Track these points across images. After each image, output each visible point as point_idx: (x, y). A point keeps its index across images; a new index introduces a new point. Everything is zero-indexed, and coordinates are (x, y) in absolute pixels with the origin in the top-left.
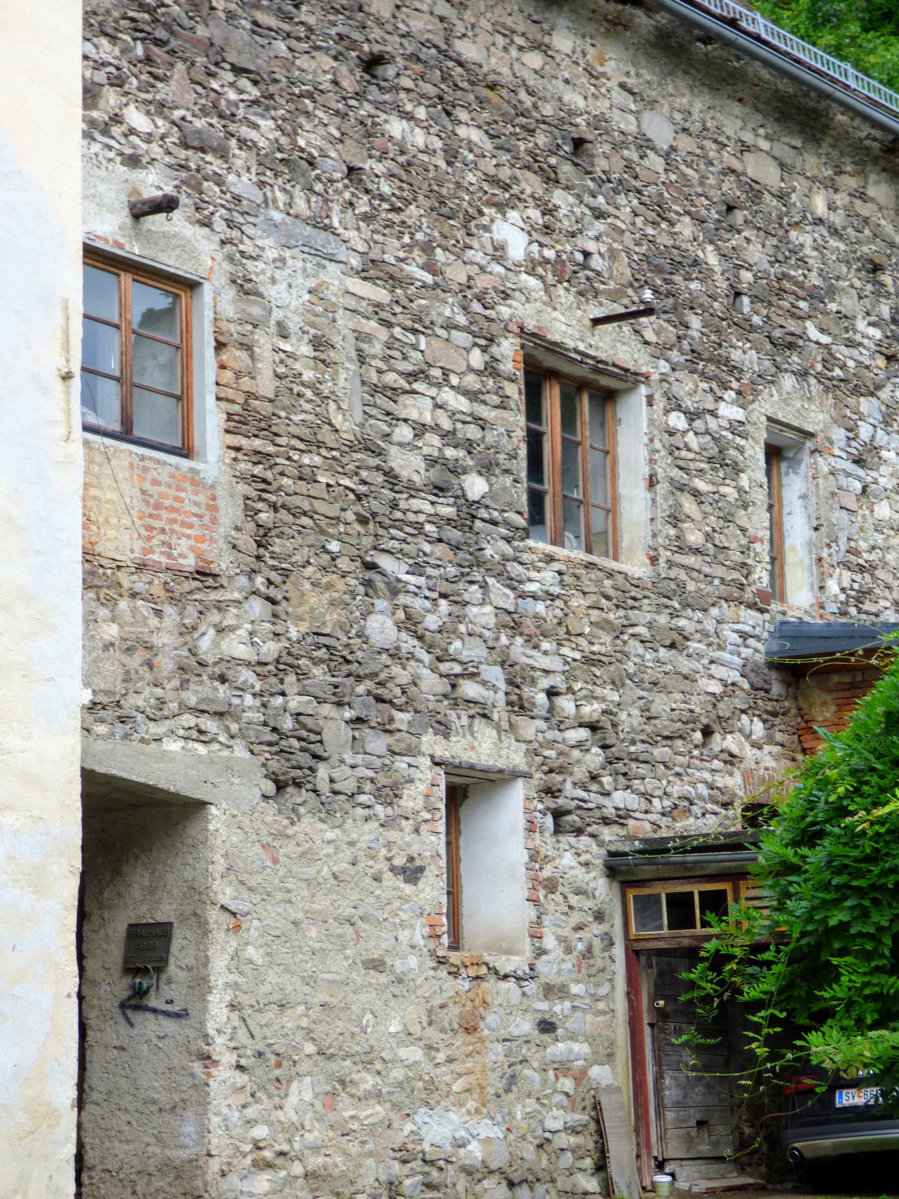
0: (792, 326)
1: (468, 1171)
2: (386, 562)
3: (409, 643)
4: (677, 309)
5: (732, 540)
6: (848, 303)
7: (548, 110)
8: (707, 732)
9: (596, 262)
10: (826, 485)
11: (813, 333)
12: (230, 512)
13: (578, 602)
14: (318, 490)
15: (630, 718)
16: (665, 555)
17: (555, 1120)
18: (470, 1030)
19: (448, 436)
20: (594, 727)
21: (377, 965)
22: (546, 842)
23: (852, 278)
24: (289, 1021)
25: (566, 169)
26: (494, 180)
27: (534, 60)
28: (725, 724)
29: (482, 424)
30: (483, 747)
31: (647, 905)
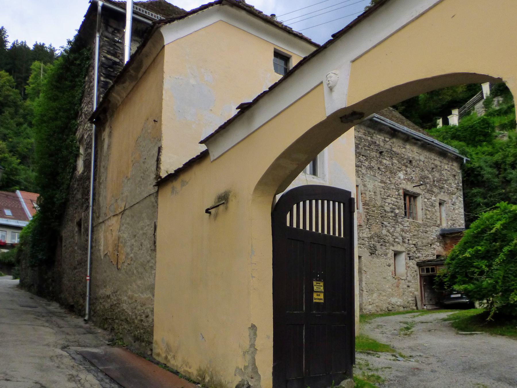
0: (442, 185)
1: (398, 306)
2: (385, 223)
3: (388, 234)
4: (425, 184)
5: (434, 217)
6: (451, 181)
7: (406, 157)
8: (431, 245)
9: (414, 178)
10: (448, 208)
11: (445, 186)
12: (363, 217)
13: (412, 227)
14: (375, 213)
15: (420, 243)
16: (424, 220)
17: (410, 299)
18: (398, 287)
19: (393, 204)
20: (414, 245)
21: (385, 278)
22: (408, 261)
23: (452, 178)
24: (373, 285)
25: (409, 165)
26: (398, 168)
27: (404, 150)
28: (433, 243)
29: (397, 202)
30: (399, 248)
31: (423, 270)
